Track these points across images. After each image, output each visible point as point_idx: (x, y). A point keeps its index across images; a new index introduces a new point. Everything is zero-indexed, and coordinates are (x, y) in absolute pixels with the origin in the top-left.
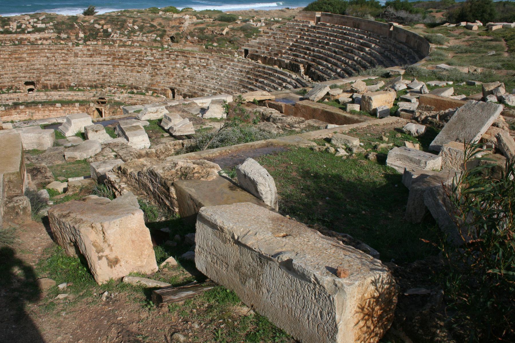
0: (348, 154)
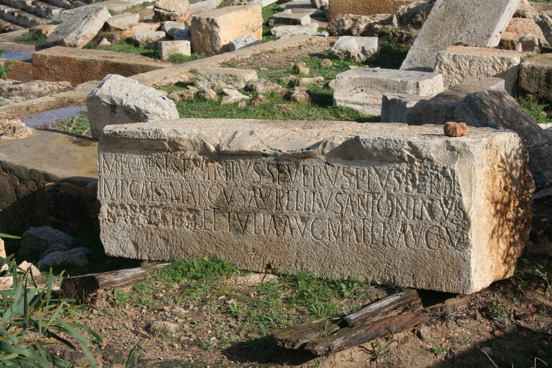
0: (247, 97)
